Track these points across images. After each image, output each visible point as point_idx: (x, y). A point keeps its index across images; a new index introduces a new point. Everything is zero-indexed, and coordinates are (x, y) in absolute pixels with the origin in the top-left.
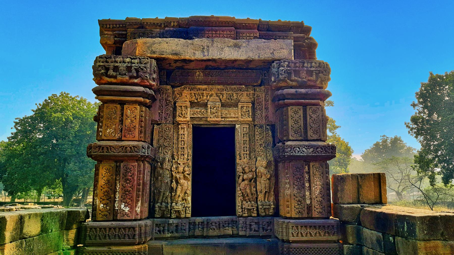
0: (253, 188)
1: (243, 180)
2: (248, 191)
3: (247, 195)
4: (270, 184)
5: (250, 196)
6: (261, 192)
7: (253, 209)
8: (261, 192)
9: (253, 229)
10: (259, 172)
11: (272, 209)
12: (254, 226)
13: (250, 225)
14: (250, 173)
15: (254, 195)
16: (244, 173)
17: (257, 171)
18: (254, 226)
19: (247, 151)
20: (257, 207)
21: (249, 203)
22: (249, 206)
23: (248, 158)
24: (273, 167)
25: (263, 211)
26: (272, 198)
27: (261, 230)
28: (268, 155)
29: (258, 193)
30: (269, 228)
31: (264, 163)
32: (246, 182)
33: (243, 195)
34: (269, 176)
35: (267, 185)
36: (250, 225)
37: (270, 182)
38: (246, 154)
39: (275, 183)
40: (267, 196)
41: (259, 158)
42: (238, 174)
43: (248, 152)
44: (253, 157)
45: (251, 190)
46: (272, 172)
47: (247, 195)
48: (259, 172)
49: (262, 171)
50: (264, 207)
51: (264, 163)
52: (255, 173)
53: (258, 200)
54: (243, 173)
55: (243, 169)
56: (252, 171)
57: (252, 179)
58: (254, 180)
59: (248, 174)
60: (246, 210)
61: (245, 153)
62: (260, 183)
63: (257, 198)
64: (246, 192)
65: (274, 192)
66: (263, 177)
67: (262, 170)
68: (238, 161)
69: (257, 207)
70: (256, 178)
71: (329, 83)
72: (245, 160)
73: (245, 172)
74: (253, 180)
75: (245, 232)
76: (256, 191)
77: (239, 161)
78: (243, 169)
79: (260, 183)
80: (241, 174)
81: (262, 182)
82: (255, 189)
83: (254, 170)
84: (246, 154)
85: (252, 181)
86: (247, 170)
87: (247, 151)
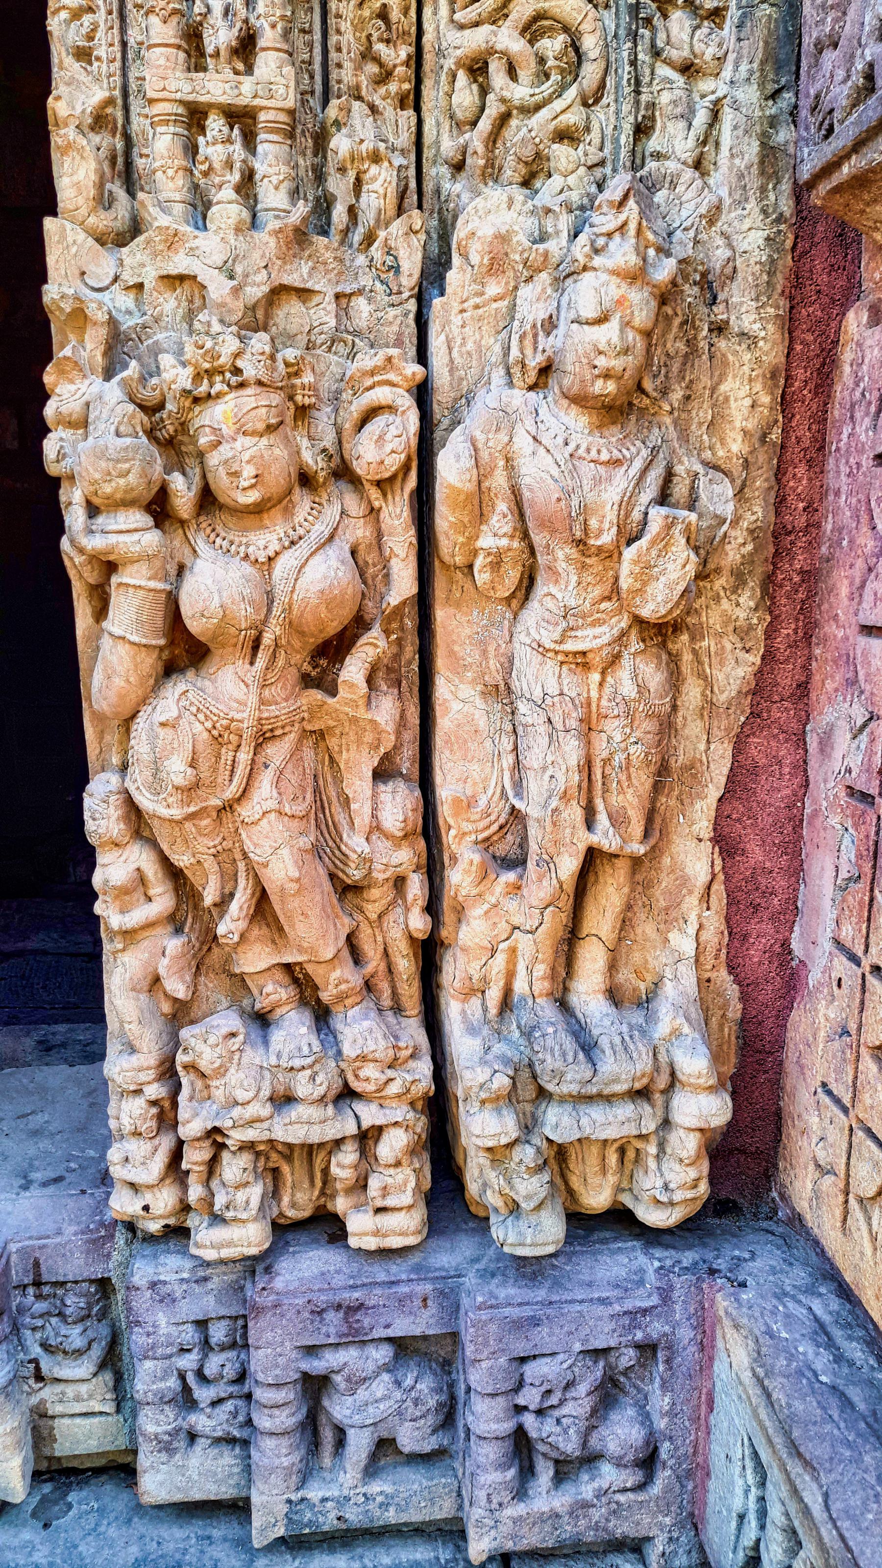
0: (359, 784)
1: (182, 651)
2: (277, 850)
3: (262, 906)
4: (667, 726)
5: (314, 932)
6: (508, 854)
7: (367, 1138)
8: (508, 854)
9: (359, 1445)
10: (478, 506)
11: (686, 1144)
12: (373, 1399)
13: (315, 1387)
14: (315, 516)
15: (377, 898)
16: (183, 502)
17: (452, 467)
18: (373, 1399)
19: (246, 47)
20: (438, 1110)
21: (294, 1031)
22: (284, 1100)
23: (272, 196)
24: (742, 397)
25: (531, 1187)
26: (682, 947)
27: (487, 1468)
28: (674, 140)
29: (459, 878)
30: (622, 1433)
31: (598, 317)
32: (231, 688)
33: (188, 908)
34: (677, 566)
35: (622, 741)
36: (315, 1387)
37: (675, 681)
38: (242, 119)
39: (760, 689)
40: (601, 920)
41: (488, 215)
42: (82, 537)
43: (273, 82)
44: (381, 183)
45: (322, 816)
46: (718, 497)
47: (262, 906)
48: (478, 506)
49: (539, 473)
50: (558, 1123)
51: (586, 295)
52: (397, 515)
53: (454, 971)
54: (159, 507)
55: (171, 439)
56: (344, 472)
57: (359, 624)
58: (391, 642)
59: (264, 540)
60: (233, 1167)
61: (217, 86)
62: (501, 692)
63: (430, 953)
64: (232, 860)
65: (725, 843)
66: (563, 587)
67: (536, 448)
68: (73, 260)
69: (438, 1110)
70: (423, 601)
71: (64, 1067)
72: (205, 252)
73: (208, 500)
74: (372, 646)
75: (227, 1460)
76: (429, 828)
77: (104, 266)
78: (171, 439)
79: (501, 692)
80: (129, 533)
81: (537, 677)
82: (397, 805)
83: (383, 447)
84: (242, 119)
85: (353, 670)
86: (238, 443)
87: (246, 47)
